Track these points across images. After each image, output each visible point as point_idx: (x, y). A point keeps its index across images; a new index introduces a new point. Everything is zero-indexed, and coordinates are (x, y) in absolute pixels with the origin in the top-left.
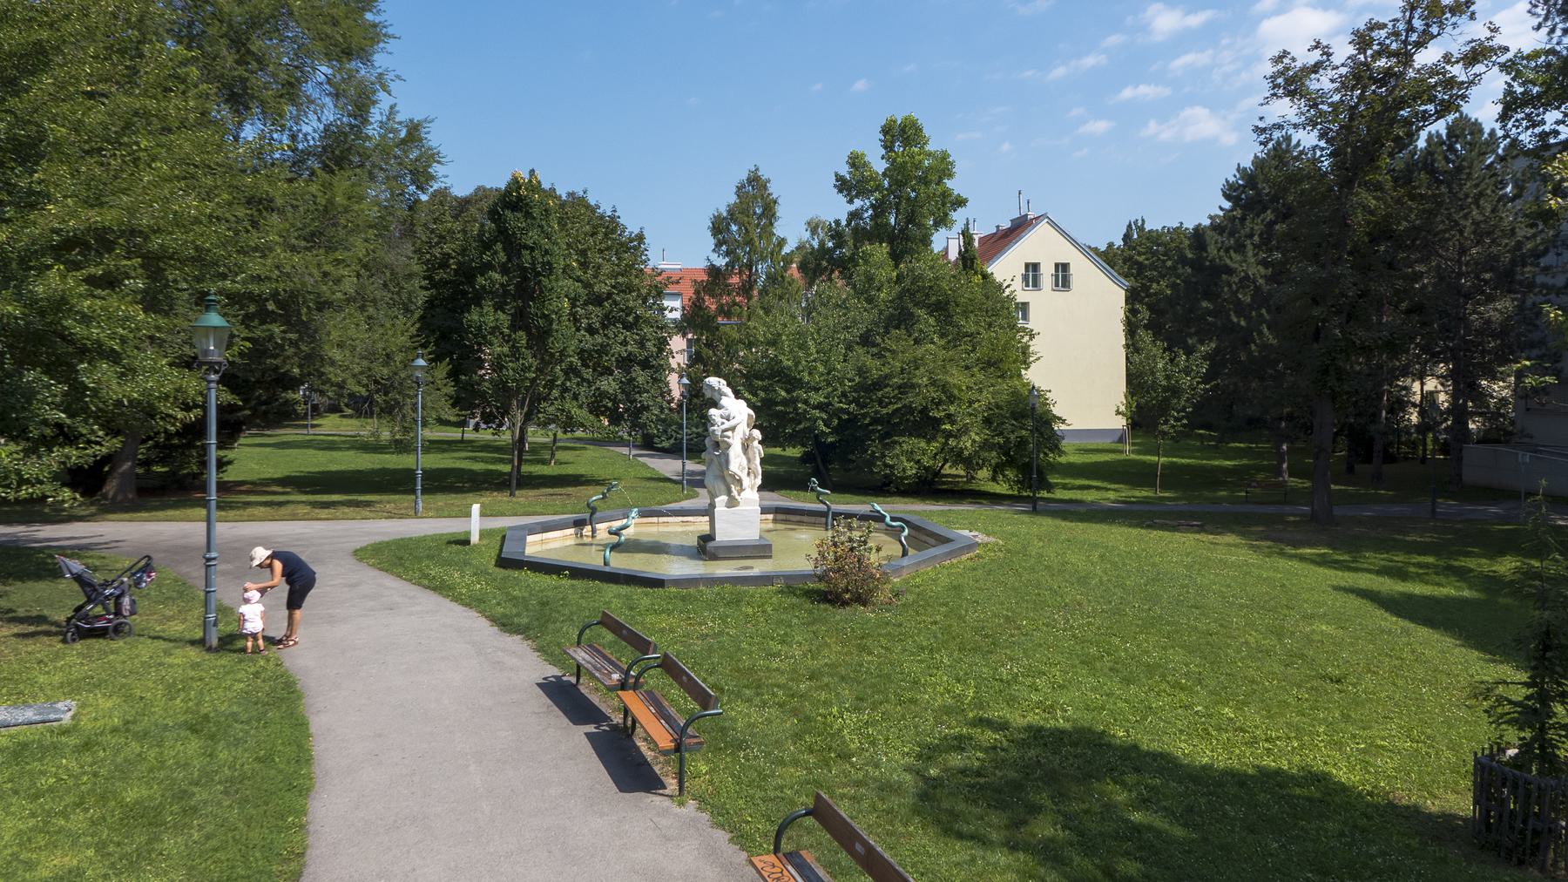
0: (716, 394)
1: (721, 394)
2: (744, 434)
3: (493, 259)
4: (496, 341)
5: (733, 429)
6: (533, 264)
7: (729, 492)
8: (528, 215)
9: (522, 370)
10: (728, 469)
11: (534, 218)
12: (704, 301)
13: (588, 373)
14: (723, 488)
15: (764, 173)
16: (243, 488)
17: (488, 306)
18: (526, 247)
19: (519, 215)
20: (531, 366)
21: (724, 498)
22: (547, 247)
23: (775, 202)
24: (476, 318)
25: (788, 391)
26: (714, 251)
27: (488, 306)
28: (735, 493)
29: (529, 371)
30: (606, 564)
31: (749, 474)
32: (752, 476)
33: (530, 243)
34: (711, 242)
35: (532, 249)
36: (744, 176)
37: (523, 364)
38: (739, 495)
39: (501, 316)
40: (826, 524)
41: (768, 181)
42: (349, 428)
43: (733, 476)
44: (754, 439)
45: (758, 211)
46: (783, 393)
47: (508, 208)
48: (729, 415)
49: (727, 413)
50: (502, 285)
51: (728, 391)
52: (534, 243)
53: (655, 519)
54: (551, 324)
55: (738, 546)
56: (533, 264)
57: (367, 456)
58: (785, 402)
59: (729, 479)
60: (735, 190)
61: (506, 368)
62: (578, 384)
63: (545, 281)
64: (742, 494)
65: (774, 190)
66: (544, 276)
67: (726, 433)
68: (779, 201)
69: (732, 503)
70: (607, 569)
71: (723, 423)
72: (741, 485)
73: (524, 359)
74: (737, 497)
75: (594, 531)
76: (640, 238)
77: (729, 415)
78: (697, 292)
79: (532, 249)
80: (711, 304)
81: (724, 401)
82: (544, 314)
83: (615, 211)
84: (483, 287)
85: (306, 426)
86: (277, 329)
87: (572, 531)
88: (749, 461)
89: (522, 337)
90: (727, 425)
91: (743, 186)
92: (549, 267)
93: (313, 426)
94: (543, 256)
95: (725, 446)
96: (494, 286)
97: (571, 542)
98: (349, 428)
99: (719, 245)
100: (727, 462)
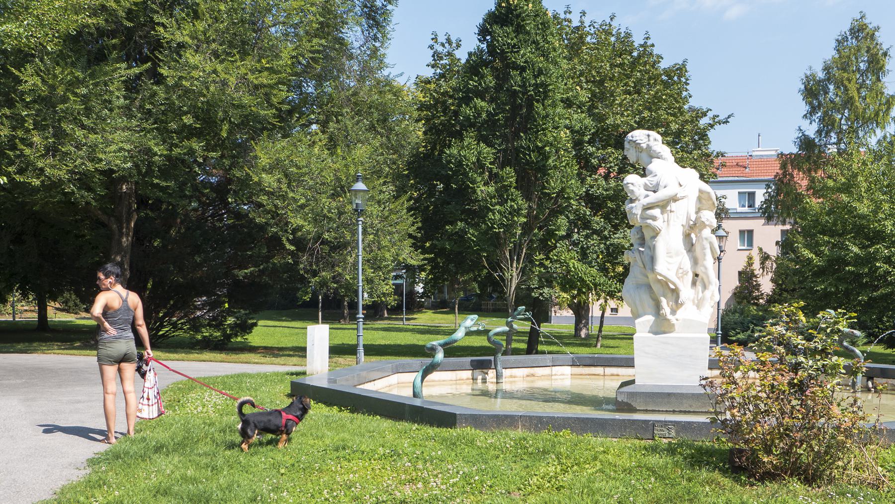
0: (644, 156)
1: (652, 155)
2: (689, 219)
3: (480, 84)
4: (479, 179)
5: (663, 205)
6: (523, 86)
7: (658, 307)
8: (520, 29)
9: (510, 213)
10: (653, 270)
11: (528, 33)
12: (792, 176)
13: (598, 221)
14: (648, 303)
15: (872, 21)
16: (285, 353)
17: (469, 139)
18: (516, 67)
19: (509, 29)
20: (520, 209)
21: (649, 319)
22: (541, 65)
23: (885, 54)
24: (455, 152)
25: (863, 247)
26: (805, 116)
27: (469, 139)
28: (666, 309)
29: (519, 215)
30: (415, 395)
31: (694, 283)
32: (699, 287)
33: (521, 62)
34: (804, 108)
35: (523, 69)
36: (846, 28)
37: (511, 206)
38: (673, 312)
39: (485, 149)
40: (854, 384)
41: (877, 29)
42: (443, 321)
43: (665, 283)
44: (704, 225)
45: (863, 66)
46: (855, 249)
47: (497, 23)
48: (658, 185)
49: (654, 180)
50: (489, 114)
51: (665, 151)
52: (526, 62)
53: (599, 370)
54: (546, 157)
55: (669, 394)
56: (523, 86)
57: (419, 336)
58: (858, 261)
59: (656, 288)
60: (834, 44)
61: (492, 211)
62: (587, 237)
63: (539, 107)
64: (679, 312)
65: (885, 39)
66: (538, 101)
67: (650, 212)
68: (890, 53)
69: (662, 326)
70: (417, 402)
71: (647, 196)
72: (678, 297)
73: (513, 200)
74: (669, 317)
75: (498, 376)
76: (680, 70)
77: (658, 185)
78: (784, 166)
79: (523, 69)
80: (802, 181)
81: (654, 166)
82: (537, 147)
83: (647, 38)
84: (467, 118)
85: (402, 319)
86: (197, 145)
87: (468, 374)
88: (695, 262)
89: (510, 175)
90: (653, 197)
91: (845, 39)
92: (543, 91)
93: (408, 319)
94: (536, 77)
95: (652, 234)
96: (479, 115)
97: (467, 388)
98: (443, 321)
99: (813, 110)
100: (653, 259)
